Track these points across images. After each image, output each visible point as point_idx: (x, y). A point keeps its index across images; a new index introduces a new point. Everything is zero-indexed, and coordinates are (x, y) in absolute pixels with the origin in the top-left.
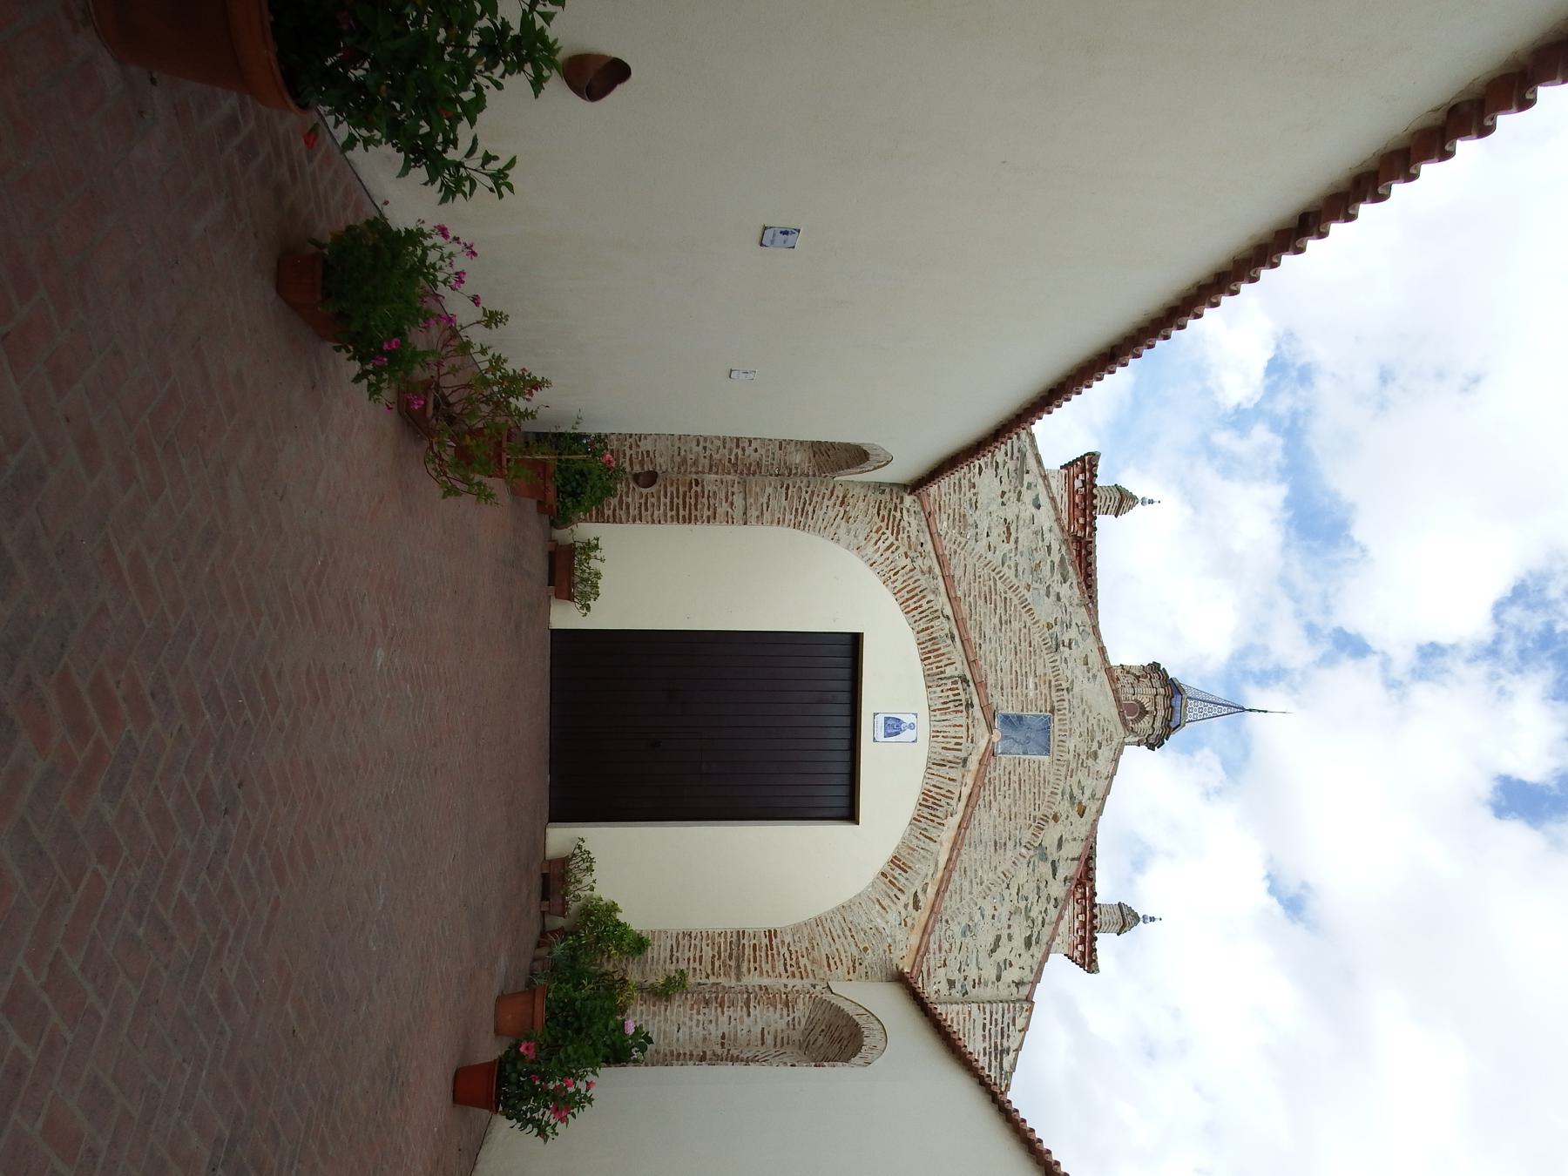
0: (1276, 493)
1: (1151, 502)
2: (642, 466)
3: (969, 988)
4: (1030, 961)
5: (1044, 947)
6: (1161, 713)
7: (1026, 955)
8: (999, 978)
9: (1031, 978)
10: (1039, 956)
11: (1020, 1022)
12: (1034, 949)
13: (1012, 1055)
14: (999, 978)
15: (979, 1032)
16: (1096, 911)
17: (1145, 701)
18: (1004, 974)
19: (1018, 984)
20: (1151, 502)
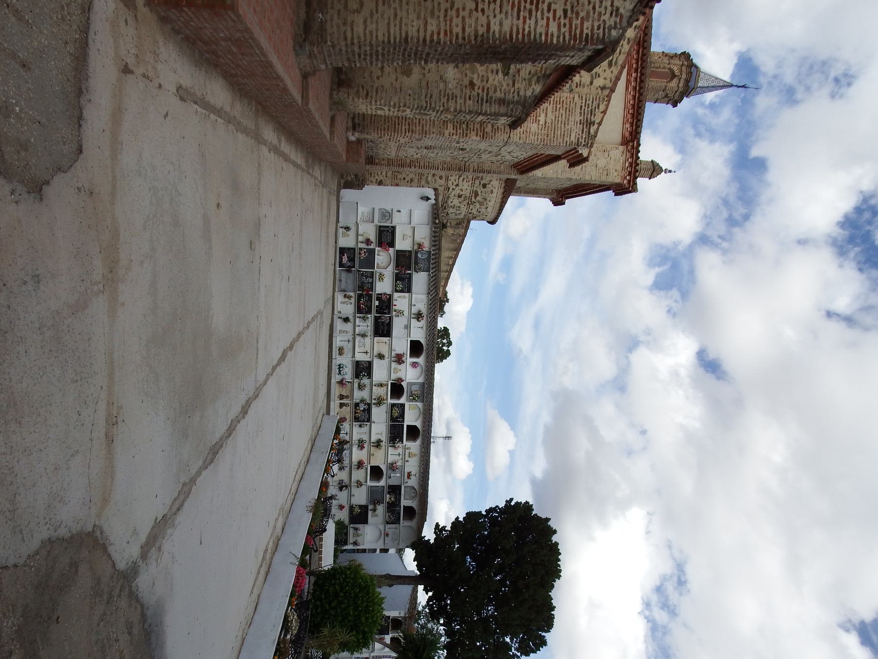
0: (732, 147)
1: (670, 171)
2: (340, 331)
3: (574, 87)
4: (610, 75)
5: (619, 67)
6: (684, 76)
7: (608, 71)
8: (591, 83)
9: (610, 85)
10: (616, 72)
11: (602, 107)
12: (613, 68)
13: (596, 126)
14: (591, 83)
15: (578, 110)
16: (638, 168)
17: (675, 69)
18: (595, 81)
19: (603, 88)
20: (670, 171)
